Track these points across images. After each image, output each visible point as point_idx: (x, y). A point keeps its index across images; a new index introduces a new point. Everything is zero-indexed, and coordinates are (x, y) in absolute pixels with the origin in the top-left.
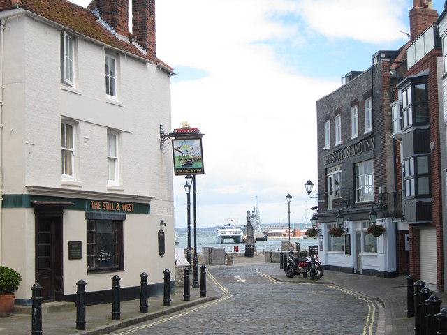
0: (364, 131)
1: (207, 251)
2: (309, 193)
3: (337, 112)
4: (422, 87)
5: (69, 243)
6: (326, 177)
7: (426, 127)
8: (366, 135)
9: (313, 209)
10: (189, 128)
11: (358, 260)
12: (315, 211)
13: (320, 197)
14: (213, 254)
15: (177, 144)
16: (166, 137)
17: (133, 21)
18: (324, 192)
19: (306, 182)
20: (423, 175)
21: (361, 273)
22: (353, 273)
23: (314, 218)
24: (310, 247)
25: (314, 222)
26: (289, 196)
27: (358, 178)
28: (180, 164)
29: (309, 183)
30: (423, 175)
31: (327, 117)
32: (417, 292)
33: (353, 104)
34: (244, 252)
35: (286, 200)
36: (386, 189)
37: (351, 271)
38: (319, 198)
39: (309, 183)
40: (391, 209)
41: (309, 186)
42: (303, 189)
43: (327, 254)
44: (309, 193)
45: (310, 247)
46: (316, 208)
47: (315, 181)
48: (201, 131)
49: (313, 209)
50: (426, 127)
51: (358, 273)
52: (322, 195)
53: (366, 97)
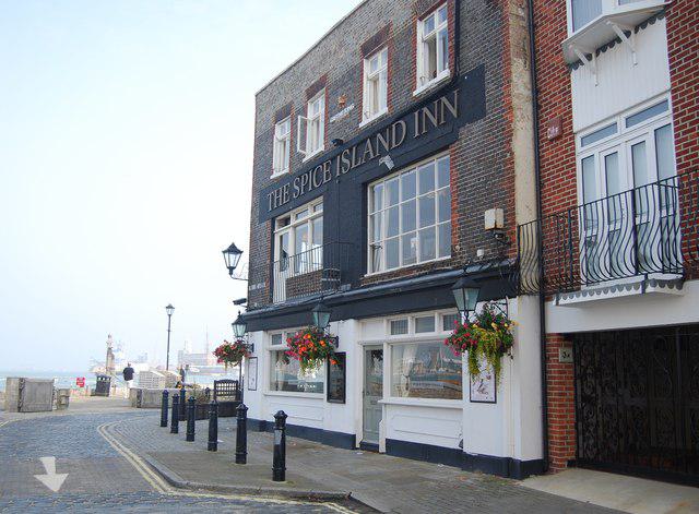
0: (360, 121)
1: (15, 384)
2: (231, 269)
5: (461, 398)
6: (273, 236)
9: (238, 302)
11: (373, 412)
12: (242, 309)
13: (253, 275)
14: (27, 389)
18: (264, 260)
19: (226, 248)
21: (382, 449)
22: (354, 448)
23: (241, 320)
24: (216, 382)
25: (241, 329)
26: (170, 307)
27: (372, 217)
29: (233, 250)
32: (215, 398)
34: (95, 387)
35: (165, 312)
37: (347, 441)
38: (251, 282)
39: (233, 250)
40: (529, 276)
41: (232, 256)
42: (220, 262)
43: (111, 369)
44: (231, 269)
45: (216, 382)
46: (243, 301)
47: (244, 244)
49: (238, 302)
51: (374, 448)
52: (261, 272)
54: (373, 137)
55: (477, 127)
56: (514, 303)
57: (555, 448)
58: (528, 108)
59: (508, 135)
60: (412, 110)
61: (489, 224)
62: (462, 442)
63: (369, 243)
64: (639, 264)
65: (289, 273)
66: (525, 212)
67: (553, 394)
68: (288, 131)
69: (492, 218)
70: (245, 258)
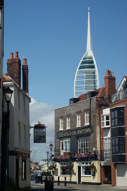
2: (51, 149)
3: (68, 116)
4: (122, 111)
6: (60, 142)
7: (124, 126)
8: (85, 126)
10: (41, 124)
15: (36, 130)
16: (31, 127)
17: (23, 81)
20: (117, 145)
28: (37, 138)
30: (117, 145)
31: (62, 118)
33: (78, 113)
36: (96, 149)
40: (99, 158)
44: (51, 149)
48: (46, 126)
50: (124, 126)
52: (57, 151)
53: (86, 111)
54: (77, 130)
55: (93, 134)
56: (97, 162)
57: (102, 181)
58: (99, 133)
59: (96, 138)
60: (83, 128)
61: (94, 150)
62: (109, 72)
63: (78, 148)
64: (107, 143)
65: (64, 151)
66: (99, 149)
67: (102, 173)
68: (88, 115)
69: (94, 149)
70: (54, 146)
